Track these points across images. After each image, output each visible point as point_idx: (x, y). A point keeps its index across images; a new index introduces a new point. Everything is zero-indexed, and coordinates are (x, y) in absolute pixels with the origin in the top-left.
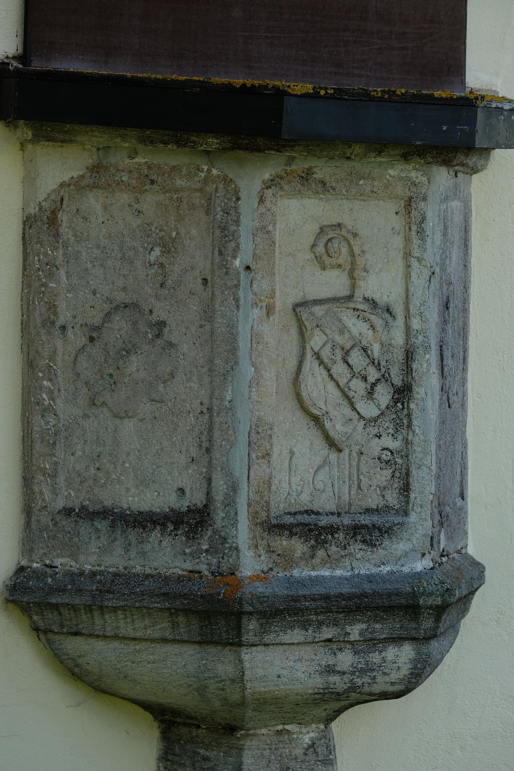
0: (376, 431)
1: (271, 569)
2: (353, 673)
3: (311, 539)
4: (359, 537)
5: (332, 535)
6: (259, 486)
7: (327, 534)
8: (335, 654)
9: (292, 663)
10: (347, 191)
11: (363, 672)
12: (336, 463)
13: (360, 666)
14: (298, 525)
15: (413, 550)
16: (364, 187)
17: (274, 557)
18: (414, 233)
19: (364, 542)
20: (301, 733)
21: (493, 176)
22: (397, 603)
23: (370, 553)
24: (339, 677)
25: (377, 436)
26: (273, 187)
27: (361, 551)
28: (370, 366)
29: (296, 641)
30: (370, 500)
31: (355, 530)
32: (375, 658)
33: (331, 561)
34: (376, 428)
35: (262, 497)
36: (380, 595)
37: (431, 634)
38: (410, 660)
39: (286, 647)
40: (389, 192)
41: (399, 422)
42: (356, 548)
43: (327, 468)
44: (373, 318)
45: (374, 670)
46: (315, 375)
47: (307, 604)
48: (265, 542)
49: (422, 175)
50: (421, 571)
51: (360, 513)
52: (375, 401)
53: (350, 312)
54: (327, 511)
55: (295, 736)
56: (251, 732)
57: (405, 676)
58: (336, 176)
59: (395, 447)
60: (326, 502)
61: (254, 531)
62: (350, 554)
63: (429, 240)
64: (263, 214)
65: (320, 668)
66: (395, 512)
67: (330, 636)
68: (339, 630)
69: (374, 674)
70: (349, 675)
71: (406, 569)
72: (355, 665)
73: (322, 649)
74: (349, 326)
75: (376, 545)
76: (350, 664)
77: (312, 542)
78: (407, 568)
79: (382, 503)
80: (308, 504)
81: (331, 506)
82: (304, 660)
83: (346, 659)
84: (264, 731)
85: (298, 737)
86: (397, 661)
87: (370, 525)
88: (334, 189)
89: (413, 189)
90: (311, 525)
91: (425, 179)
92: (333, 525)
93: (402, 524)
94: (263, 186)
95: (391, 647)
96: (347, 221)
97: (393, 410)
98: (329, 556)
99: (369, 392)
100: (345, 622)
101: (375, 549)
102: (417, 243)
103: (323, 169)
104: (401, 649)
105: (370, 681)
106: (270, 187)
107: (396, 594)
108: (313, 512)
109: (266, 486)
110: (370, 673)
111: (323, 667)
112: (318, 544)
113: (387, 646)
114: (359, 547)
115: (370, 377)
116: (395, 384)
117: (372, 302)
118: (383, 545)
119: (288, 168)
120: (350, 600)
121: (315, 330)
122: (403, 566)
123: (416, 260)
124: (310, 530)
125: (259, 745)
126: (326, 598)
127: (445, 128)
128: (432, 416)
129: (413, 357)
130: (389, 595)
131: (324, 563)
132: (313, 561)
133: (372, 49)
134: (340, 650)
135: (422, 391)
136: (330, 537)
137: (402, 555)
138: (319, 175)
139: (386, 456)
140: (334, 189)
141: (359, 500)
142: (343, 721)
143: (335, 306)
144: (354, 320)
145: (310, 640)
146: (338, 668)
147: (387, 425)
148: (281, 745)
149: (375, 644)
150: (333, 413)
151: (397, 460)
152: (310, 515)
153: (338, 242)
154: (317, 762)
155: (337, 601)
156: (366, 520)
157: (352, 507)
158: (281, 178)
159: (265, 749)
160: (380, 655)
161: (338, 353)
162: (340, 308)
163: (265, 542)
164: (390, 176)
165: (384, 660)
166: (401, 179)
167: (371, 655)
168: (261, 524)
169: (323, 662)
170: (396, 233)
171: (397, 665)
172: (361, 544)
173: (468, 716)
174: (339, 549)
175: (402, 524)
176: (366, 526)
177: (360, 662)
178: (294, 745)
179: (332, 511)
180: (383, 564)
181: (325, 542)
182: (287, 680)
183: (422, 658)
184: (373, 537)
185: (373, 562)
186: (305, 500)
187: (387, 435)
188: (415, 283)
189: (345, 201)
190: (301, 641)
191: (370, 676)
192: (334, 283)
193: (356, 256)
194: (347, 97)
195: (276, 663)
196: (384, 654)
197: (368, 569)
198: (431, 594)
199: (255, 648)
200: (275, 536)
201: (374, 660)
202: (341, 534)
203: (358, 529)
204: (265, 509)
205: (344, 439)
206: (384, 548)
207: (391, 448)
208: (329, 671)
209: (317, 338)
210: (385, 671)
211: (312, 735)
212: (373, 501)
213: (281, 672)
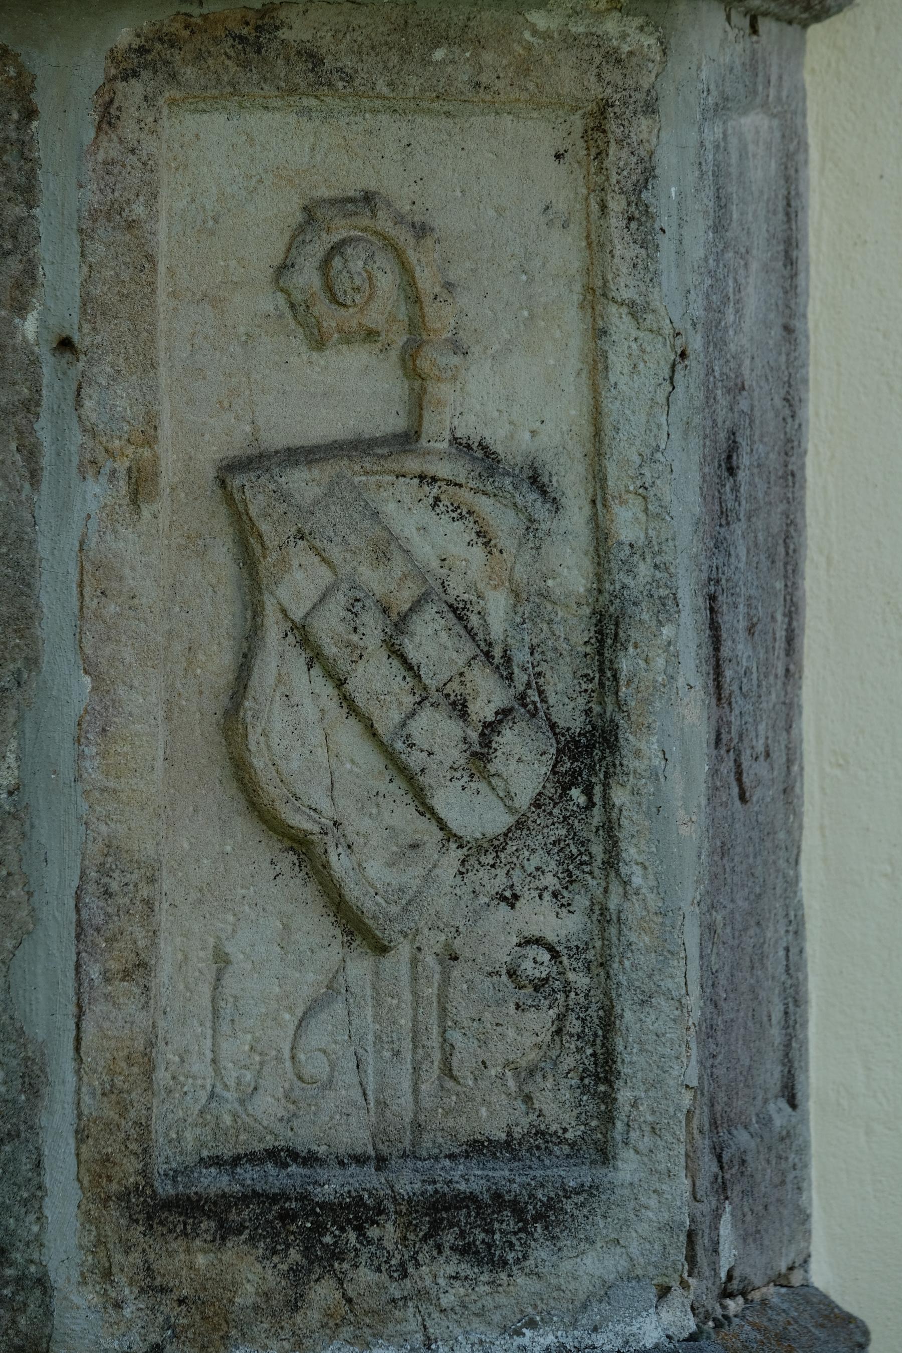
0: (499, 882)
3: (288, 1246)
4: (449, 1237)
5: (360, 1230)
6: (111, 1072)
7: (342, 1229)
10: (391, 84)
12: (369, 992)
14: (245, 1199)
15: (630, 1277)
16: (449, 69)
17: (168, 1307)
19: (465, 1251)
23: (487, 1288)
25: (504, 899)
27: (457, 1284)
28: (477, 666)
30: (484, 1111)
31: (436, 1214)
34: (501, 872)
35: (123, 1109)
40: (531, 87)
42: (438, 1272)
44: (485, 505)
46: (295, 699)
48: (135, 1257)
49: (641, 29)
51: (451, 1157)
53: (407, 489)
54: (342, 1151)
59: (563, 933)
60: (339, 1122)
61: (98, 1223)
62: (422, 1294)
63: (667, 244)
64: (113, 162)
66: (566, 1149)
74: (407, 533)
75: (505, 1263)
77: (294, 1255)
79: (525, 1121)
80: (279, 1128)
81: (355, 1135)
87: (486, 1197)
88: (348, 78)
89: (613, 75)
90: (288, 1199)
91: (652, 41)
92: (361, 1198)
93: (591, 1191)
94: (113, 71)
97: (556, 811)
98: (349, 1301)
99: (474, 754)
101: (503, 1276)
106: (135, 74)
108: (293, 1155)
109: (135, 1069)
112: (311, 1263)
114: (450, 1270)
116: (561, 723)
118: (531, 1262)
122: (595, 1329)
124: (286, 1217)
128: (684, 830)
135: (650, 746)
137: (594, 1294)
139: (537, 964)
140: (348, 78)
141: (446, 1114)
143: (357, 468)
144: (423, 514)
147: (535, 861)
150: (357, 823)
151: (571, 976)
152: (286, 1166)
153: (364, 256)
156: (471, 1178)
157: (426, 1136)
158: (173, 42)
163: (135, 1257)
164: (535, 33)
166: (571, 41)
168: (123, 1197)
172: (455, 1258)
174: (384, 1277)
175: (591, 1191)
176: (472, 1197)
179: (359, 1151)
180: (532, 1324)
181: (336, 1254)
184: (497, 1236)
185: (496, 1318)
186: (268, 1113)
187: (535, 894)
188: (621, 386)
189: (385, 118)
192: (353, 391)
200: (170, 1237)
202: (390, 1226)
203: (447, 1209)
204: (134, 1146)
205: (394, 909)
207: (551, 938)
212: (496, 1115)
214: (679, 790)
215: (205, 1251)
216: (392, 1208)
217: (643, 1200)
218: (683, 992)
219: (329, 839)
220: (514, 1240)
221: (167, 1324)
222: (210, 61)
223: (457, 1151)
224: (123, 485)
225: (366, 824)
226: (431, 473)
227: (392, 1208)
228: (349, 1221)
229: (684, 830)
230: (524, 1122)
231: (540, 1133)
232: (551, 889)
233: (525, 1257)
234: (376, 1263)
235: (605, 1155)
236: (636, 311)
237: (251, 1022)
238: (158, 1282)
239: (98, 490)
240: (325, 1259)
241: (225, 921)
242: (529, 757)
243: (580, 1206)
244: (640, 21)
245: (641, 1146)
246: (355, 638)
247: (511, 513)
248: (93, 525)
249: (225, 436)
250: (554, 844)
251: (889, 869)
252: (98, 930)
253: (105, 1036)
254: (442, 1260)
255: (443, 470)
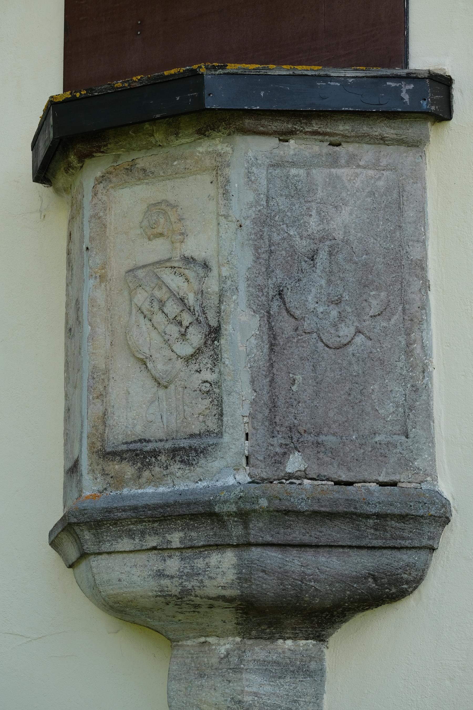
0: (196, 367)
1: (106, 489)
2: (180, 577)
3: (137, 462)
4: (178, 458)
5: (155, 457)
6: (94, 422)
7: (151, 458)
8: (165, 560)
9: (128, 569)
10: (164, 172)
11: (189, 576)
12: (164, 398)
13: (186, 571)
14: (127, 451)
15: (227, 467)
16: (178, 166)
17: (109, 479)
18: (220, 195)
19: (182, 461)
20: (219, 645)
21: (452, 144)
22: (196, 511)
23: (188, 471)
24: (169, 581)
25: (197, 371)
26: (103, 182)
27: (180, 470)
28: (184, 312)
29: (128, 549)
30: (193, 426)
31: (174, 452)
32: (200, 563)
33: (155, 481)
34: (197, 365)
35: (97, 430)
36: (181, 504)
37: (243, 541)
38: (233, 565)
39: (125, 555)
40: (199, 166)
41: (216, 357)
42: (175, 467)
43: (157, 403)
44: (187, 272)
45: (199, 574)
46: (140, 326)
47: (119, 514)
48: (100, 467)
49: (227, 146)
50: (233, 485)
51: (185, 438)
52: (188, 340)
53: (168, 271)
54: (157, 439)
55: (214, 647)
56: (180, 643)
57: (233, 580)
58: (154, 163)
59: (212, 379)
60: (156, 431)
61: (91, 458)
62: (171, 473)
63: (234, 200)
64: (96, 204)
65: (152, 573)
66: (215, 435)
67: (155, 544)
68: (161, 539)
69: (201, 578)
70: (177, 579)
71: (219, 484)
72: (182, 570)
73: (154, 557)
74: (168, 282)
75: (193, 464)
76: (177, 568)
77: (139, 464)
78: (221, 482)
79: (204, 428)
80: (142, 434)
81: (161, 435)
82: (138, 566)
83: (173, 565)
84: (189, 643)
85: (216, 649)
86: (220, 566)
87: (187, 448)
88: (153, 173)
89: (219, 159)
90: (137, 451)
91: (230, 149)
92: (155, 449)
93: (216, 445)
94: (96, 183)
95: (215, 554)
96: (171, 198)
97: (211, 348)
98: (153, 476)
99: (182, 335)
100: (163, 531)
101: (192, 468)
102: (223, 203)
103: (144, 160)
104: (224, 555)
105: (198, 584)
106: (101, 182)
107: (195, 503)
108: (145, 440)
109: (99, 420)
110: (197, 577)
111: (155, 571)
112: (143, 466)
113: (211, 553)
114: (178, 467)
115: (185, 322)
116: (212, 325)
117: (191, 260)
118: (200, 464)
119: (115, 165)
120: (155, 510)
121: (138, 289)
122: (217, 481)
123: (223, 217)
124: (137, 455)
125: (183, 654)
126: (135, 508)
127: (178, 99)
128: (241, 349)
129: (221, 300)
130: (189, 504)
131: (149, 482)
132: (140, 481)
133: (322, 62)
134: (170, 557)
135: (230, 327)
136: (153, 459)
137: (217, 472)
138: (141, 164)
139: (206, 387)
140: (153, 173)
141: (183, 428)
142: (338, 651)
143: (155, 267)
144: (173, 277)
145: (138, 548)
146: (167, 573)
147: (206, 361)
148: (201, 655)
149: (201, 551)
150: (156, 355)
151: (215, 390)
152: (143, 443)
153: (156, 215)
154: (229, 670)
155: (144, 511)
156: (184, 443)
157: (178, 434)
158: (111, 173)
159: (188, 657)
160: (204, 561)
161: (156, 305)
162: (159, 268)
163: (100, 467)
164: (199, 153)
165: (208, 565)
166: (208, 153)
167: (195, 561)
168: (97, 452)
169: (155, 568)
170: (212, 199)
171: (221, 570)
172: (179, 464)
173: (455, 648)
174: (162, 469)
175: (216, 445)
176: (184, 448)
177: (186, 567)
178: (211, 655)
179: (161, 438)
180: (200, 480)
181: (150, 464)
182: (127, 583)
183: (245, 564)
184: (190, 457)
185: (192, 479)
186: (139, 430)
187: (206, 369)
188: (223, 237)
189: (168, 181)
190: (131, 549)
191: (197, 580)
192: (159, 249)
193: (173, 223)
194: (97, 94)
195: (117, 568)
196: (207, 560)
197: (187, 485)
198: (225, 502)
199: (101, 556)
200: (108, 461)
201: (199, 566)
202: (163, 456)
203: (177, 451)
204: (99, 439)
205: (164, 376)
206: (200, 467)
207: (209, 380)
208: (160, 575)
209: (139, 295)
210: (211, 575)
211: (228, 646)
212: (196, 428)
213: (120, 576)
214: (239, 338)
215: (118, 465)
216: (163, 452)
217: (231, 446)
218: (241, 391)
219: (148, 360)
220: (195, 458)
221: (108, 483)
222: (119, 176)
223: (186, 437)
224: (98, 280)
225: (158, 355)
226: (173, 266)
227: (163, 452)
228: (153, 455)
229: (241, 349)
230: (203, 429)
231: (208, 431)
232: (210, 368)
233: (198, 463)
234: (160, 466)
235: (220, 434)
236: (226, 217)
237: (135, 408)
238: (106, 472)
239: (92, 282)
240: (147, 465)
241: (129, 384)
242: (197, 334)
243: (213, 449)
244: (226, 144)
245: (230, 433)
246: (152, 309)
247: (193, 273)
248: (91, 290)
249: (130, 264)
250: (211, 356)
251: (464, 374)
252: (91, 387)
253: (93, 413)
254: (176, 464)
255: (176, 265)
